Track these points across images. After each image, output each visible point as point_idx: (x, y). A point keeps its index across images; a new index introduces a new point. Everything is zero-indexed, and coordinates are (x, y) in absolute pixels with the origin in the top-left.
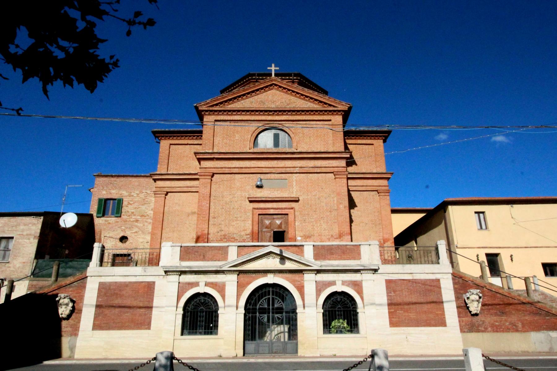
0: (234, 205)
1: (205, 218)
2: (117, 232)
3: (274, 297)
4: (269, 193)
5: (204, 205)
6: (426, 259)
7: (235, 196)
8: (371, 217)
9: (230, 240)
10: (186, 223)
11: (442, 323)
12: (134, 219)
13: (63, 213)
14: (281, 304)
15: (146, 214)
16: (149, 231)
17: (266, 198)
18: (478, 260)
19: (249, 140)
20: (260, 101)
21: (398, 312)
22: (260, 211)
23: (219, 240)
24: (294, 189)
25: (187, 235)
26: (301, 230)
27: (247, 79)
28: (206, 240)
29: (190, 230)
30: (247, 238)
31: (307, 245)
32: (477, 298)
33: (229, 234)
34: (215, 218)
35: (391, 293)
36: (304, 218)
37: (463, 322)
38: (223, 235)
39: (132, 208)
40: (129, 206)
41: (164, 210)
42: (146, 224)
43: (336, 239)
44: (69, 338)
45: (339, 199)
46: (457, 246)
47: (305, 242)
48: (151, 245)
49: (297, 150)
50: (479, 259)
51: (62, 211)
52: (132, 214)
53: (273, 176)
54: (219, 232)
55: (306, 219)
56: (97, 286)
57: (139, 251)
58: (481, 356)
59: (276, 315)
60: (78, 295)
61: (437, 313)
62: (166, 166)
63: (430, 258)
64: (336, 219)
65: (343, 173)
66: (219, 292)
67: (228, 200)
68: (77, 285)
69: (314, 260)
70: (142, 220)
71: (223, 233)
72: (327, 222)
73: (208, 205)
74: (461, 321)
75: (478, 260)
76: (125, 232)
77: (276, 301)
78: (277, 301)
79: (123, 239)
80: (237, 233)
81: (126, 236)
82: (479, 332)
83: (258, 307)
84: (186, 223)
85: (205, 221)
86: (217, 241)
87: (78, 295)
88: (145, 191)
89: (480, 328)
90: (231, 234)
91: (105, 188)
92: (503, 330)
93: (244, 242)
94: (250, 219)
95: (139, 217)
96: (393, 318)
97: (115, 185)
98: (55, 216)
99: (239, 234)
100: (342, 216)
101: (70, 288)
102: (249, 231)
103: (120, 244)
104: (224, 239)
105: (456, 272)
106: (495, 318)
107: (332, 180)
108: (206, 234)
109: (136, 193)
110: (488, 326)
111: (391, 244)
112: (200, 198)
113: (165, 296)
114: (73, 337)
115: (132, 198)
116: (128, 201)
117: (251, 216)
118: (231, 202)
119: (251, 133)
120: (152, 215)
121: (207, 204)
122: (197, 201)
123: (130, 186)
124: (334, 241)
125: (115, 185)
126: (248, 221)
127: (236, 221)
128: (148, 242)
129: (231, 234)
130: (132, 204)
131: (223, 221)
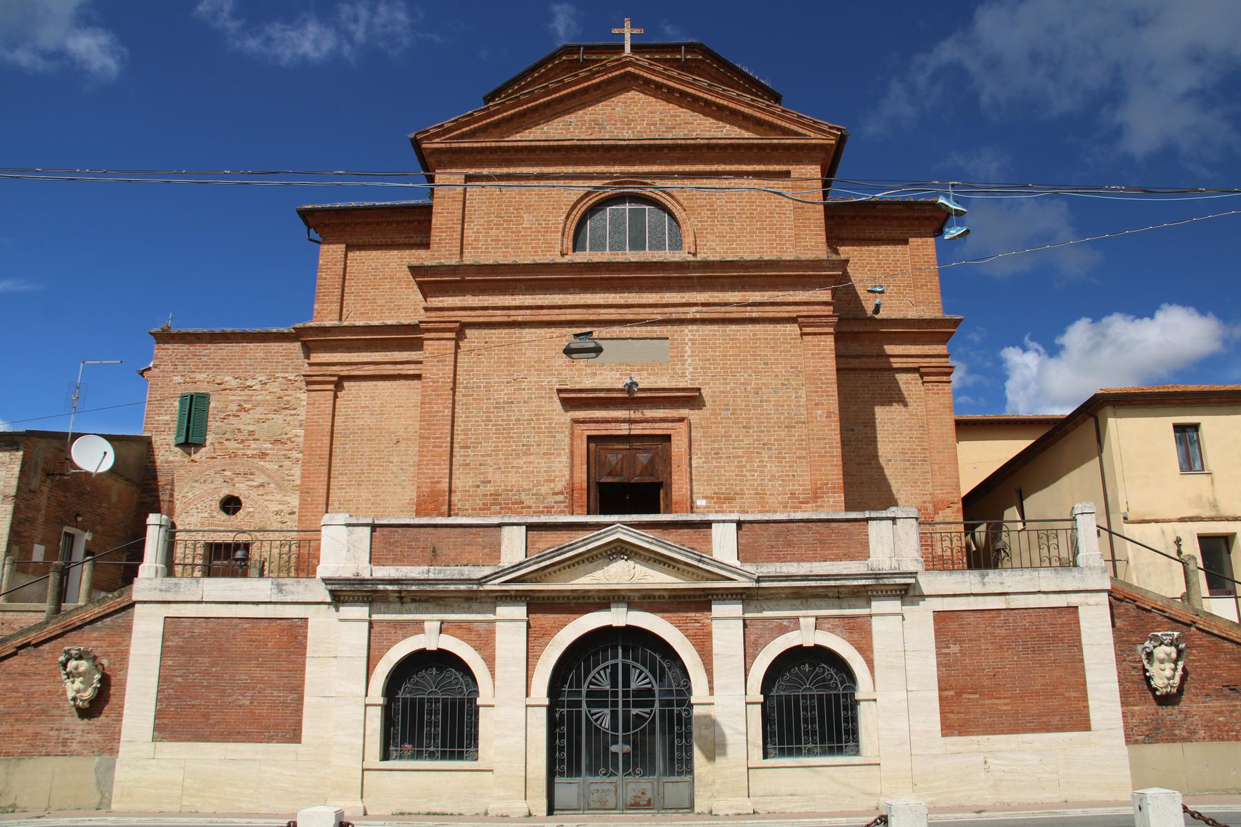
0: (520, 411)
1: (441, 447)
2: (212, 486)
3: (630, 661)
4: (618, 376)
5: (437, 412)
6: (1045, 552)
7: (524, 385)
8: (902, 442)
9: (510, 508)
10: (392, 462)
11: (1080, 722)
12: (254, 449)
13: (76, 436)
14: (647, 680)
15: (286, 437)
16: (295, 483)
17: (609, 390)
18: (1179, 552)
19: (561, 229)
20: (591, 121)
21: (965, 696)
22: (593, 426)
23: (481, 509)
24: (686, 366)
25: (395, 493)
26: (707, 481)
27: (557, 62)
28: (446, 508)
29: (404, 481)
30: (555, 502)
31: (719, 522)
32: (1172, 651)
33: (507, 490)
34: (469, 447)
35: (949, 648)
36: (716, 446)
37: (1133, 716)
38: (491, 495)
39: (249, 421)
40: (242, 414)
41: (333, 426)
42: (287, 463)
43: (802, 503)
44: (97, 759)
45: (810, 392)
46: (1125, 518)
47: (717, 512)
48: (300, 520)
49: (695, 255)
50: (1183, 548)
51: (70, 429)
52: (251, 438)
53: (626, 331)
54: (478, 486)
55: (721, 449)
56: (159, 627)
57: (272, 536)
58: (1182, 810)
59: (634, 711)
60: (114, 649)
61: (1067, 694)
62: (336, 307)
63: (1054, 552)
64: (804, 449)
65: (824, 320)
66: (477, 648)
67: (502, 397)
68: (110, 623)
69: (737, 564)
70: (275, 452)
71: (490, 488)
72: (780, 458)
73: (448, 412)
74: (1129, 714)
75: (1179, 552)
76: (234, 485)
77: (634, 674)
78: (638, 671)
79: (231, 505)
80: (529, 490)
81: (236, 495)
82: (1174, 741)
83: (584, 690)
84: (392, 462)
85: (442, 456)
86: (476, 511)
87: (114, 649)
88: (282, 375)
89: (1177, 732)
90: (512, 490)
91: (181, 368)
92: (1237, 736)
93: (549, 512)
94: (564, 449)
95: (269, 446)
96: (952, 712)
97: (205, 359)
98: (56, 443)
99: (535, 492)
100: (821, 439)
101: (93, 631)
102: (561, 485)
103: (223, 516)
104: (494, 504)
105: (1119, 586)
106: (1217, 704)
107: (791, 339)
108: (444, 491)
109: (260, 379)
110: (1197, 725)
111: (954, 514)
112: (424, 399)
113: (336, 657)
114: (106, 756)
115: (251, 393)
116: (239, 400)
117: (567, 440)
118: (512, 403)
119: (566, 209)
120: (301, 439)
121: (447, 408)
122: (418, 399)
123: (242, 362)
124: (801, 507)
125: (205, 359)
126: (559, 455)
127: (525, 454)
128: (292, 513)
129: (512, 490)
130: (249, 409)
131: (490, 455)
